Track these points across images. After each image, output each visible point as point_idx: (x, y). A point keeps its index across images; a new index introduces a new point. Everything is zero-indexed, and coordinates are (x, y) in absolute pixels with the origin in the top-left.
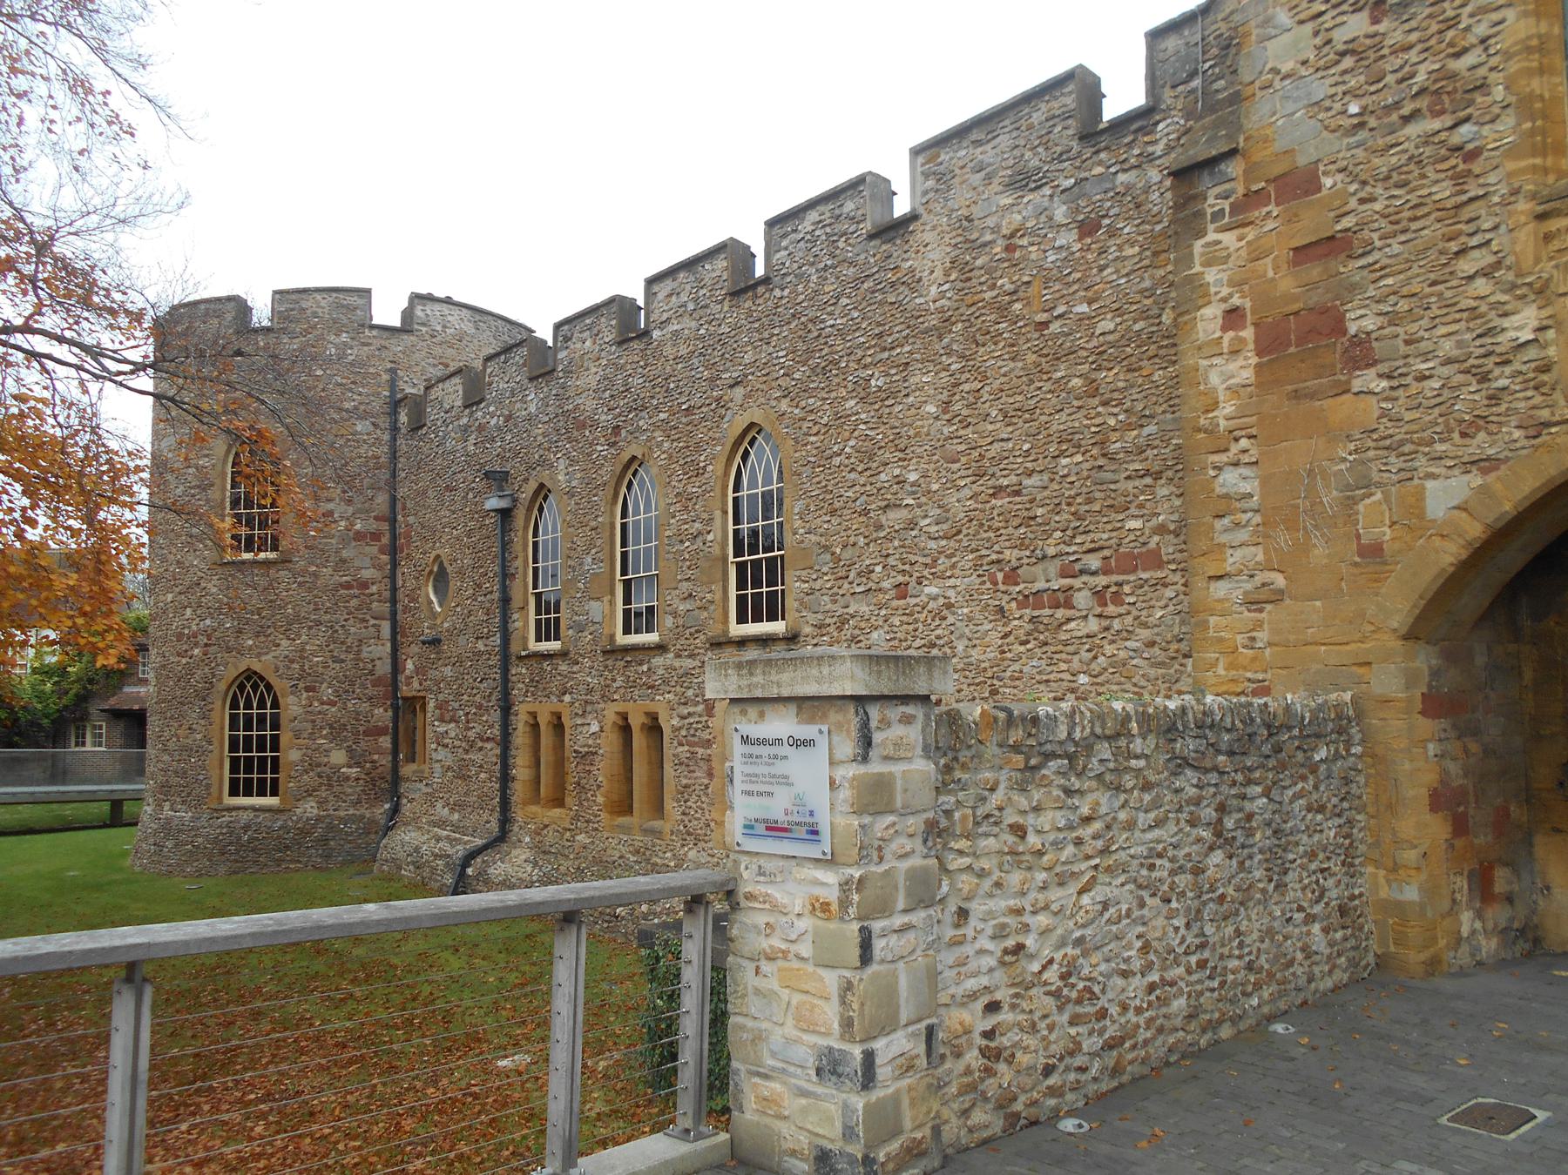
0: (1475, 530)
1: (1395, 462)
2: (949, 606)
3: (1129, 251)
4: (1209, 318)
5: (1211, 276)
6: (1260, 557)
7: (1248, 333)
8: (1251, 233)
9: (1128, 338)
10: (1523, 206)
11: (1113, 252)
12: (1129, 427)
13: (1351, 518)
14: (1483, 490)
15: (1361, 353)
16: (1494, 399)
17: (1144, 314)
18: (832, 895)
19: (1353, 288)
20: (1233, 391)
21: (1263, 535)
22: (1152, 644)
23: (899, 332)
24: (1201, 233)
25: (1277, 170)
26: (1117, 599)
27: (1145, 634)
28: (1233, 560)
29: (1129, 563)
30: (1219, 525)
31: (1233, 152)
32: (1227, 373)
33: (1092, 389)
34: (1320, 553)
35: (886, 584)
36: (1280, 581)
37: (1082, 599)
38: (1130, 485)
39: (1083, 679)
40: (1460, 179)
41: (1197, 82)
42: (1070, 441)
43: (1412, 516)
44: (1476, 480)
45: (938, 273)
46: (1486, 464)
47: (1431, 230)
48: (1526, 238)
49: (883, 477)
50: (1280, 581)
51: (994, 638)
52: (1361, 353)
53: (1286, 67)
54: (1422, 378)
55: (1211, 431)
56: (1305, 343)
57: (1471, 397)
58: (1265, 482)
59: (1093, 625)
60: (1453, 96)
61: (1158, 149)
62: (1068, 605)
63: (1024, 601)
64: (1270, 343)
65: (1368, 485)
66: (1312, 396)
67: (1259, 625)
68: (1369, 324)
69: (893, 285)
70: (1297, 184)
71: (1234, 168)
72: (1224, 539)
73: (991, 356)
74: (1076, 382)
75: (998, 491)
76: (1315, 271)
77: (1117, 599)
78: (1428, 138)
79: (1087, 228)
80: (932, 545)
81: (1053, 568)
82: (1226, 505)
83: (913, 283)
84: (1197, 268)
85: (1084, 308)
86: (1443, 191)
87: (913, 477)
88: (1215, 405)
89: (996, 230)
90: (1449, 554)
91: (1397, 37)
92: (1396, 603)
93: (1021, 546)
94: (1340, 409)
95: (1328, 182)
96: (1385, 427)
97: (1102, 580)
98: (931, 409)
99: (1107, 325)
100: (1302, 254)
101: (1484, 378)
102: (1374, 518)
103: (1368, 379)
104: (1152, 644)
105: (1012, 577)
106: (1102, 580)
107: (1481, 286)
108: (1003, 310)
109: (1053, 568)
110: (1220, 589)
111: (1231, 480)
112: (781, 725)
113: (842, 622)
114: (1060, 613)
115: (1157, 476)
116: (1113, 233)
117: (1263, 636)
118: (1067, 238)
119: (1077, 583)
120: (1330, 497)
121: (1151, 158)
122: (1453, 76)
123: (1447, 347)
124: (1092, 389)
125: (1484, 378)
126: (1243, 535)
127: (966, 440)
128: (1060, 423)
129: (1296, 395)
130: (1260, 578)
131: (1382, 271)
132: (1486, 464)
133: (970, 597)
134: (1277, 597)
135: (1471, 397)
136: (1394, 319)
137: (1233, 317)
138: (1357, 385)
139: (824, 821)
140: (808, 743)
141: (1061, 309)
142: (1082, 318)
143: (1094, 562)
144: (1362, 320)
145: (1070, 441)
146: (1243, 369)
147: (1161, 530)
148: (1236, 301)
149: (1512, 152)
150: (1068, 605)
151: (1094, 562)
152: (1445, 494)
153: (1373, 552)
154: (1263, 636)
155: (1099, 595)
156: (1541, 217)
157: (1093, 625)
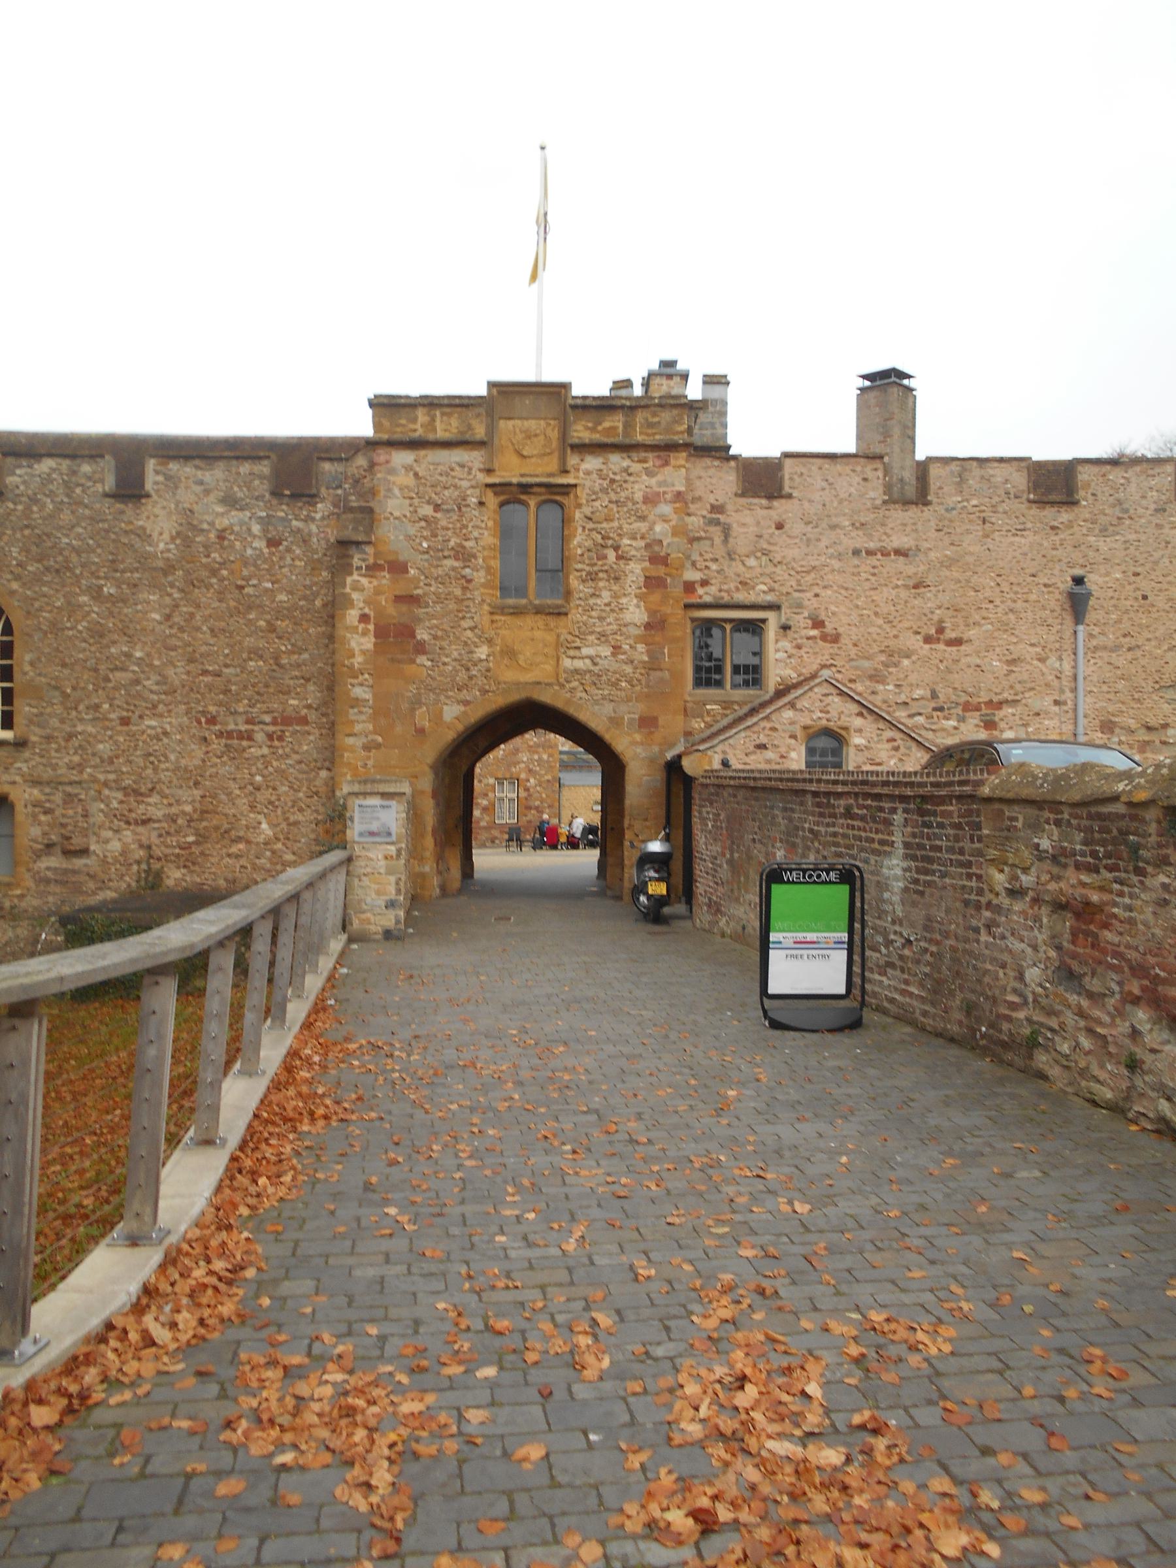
0: (460, 727)
1: (432, 696)
2: (165, 733)
3: (298, 563)
4: (352, 616)
5: (355, 596)
6: (371, 727)
7: (371, 627)
8: (375, 583)
9: (295, 607)
10: (486, 607)
11: (288, 561)
12: (294, 653)
13: (413, 716)
14: (465, 713)
15: (421, 648)
16: (471, 678)
17: (304, 598)
18: (394, 853)
19: (420, 620)
20: (363, 652)
21: (374, 717)
22: (300, 762)
23: (130, 561)
24: (351, 574)
25: (391, 558)
26: (281, 739)
27: (296, 757)
28: (358, 728)
29: (287, 721)
30: (351, 711)
31: (369, 543)
32: (360, 643)
33: (272, 628)
34: (399, 729)
35: (113, 716)
36: (380, 739)
37: (260, 737)
38: (291, 682)
39: (258, 778)
40: (464, 589)
41: (339, 492)
42: (256, 653)
43: (438, 717)
44: (462, 708)
45: (166, 536)
46: (466, 703)
47: (452, 606)
48: (486, 619)
49: (113, 650)
50: (380, 739)
51: (200, 754)
52: (421, 648)
53: (397, 514)
54: (445, 664)
55: (351, 667)
56: (396, 638)
57: (462, 676)
58: (375, 695)
59: (265, 751)
60: (463, 555)
61: (318, 516)
62: (250, 738)
63: (220, 735)
64: (381, 633)
65: (420, 703)
66: (399, 662)
67: (369, 758)
68: (426, 637)
69: (126, 532)
70: (398, 568)
71: (370, 550)
72: (352, 718)
73: (206, 597)
74: (262, 623)
75: (205, 672)
76: (404, 608)
77: (281, 739)
78: (454, 569)
79: (273, 543)
80: (155, 697)
81: (240, 719)
82: (356, 702)
83: (144, 536)
84: (348, 590)
85: (269, 585)
86: (458, 592)
87: (138, 654)
88: (353, 656)
89: (212, 524)
90: (450, 735)
91: (444, 523)
92: (430, 752)
93: (220, 704)
94: (410, 669)
95: (412, 572)
96: (429, 681)
97: (271, 728)
98: (157, 617)
99: (283, 597)
100: (398, 599)
101: (468, 669)
102: (422, 717)
103: (422, 660)
104: (300, 762)
105: (212, 721)
106: (271, 728)
107: (469, 633)
108: (214, 573)
109: (240, 719)
110: (350, 741)
111: (359, 692)
112: (375, 801)
113: (70, 737)
114: (245, 743)
115: (308, 680)
116: (288, 550)
117: (370, 763)
118: (260, 544)
119: (256, 728)
120: (405, 706)
121: (313, 519)
122: (464, 547)
123: (455, 654)
124: (272, 628)
125: (468, 669)
126: (363, 717)
127: (181, 639)
128: (249, 642)
129: (392, 660)
130: (370, 737)
131: (433, 617)
132: (466, 703)
133: (181, 729)
134: (378, 746)
135: (462, 676)
136: (435, 637)
137: (364, 618)
138: (418, 661)
139: (394, 830)
140: (388, 807)
141: (254, 582)
142: (267, 590)
143: (267, 718)
144: (422, 634)
145: (256, 653)
146: (368, 643)
147: (309, 707)
148: (367, 610)
149: (484, 586)
150: (250, 738)
151: (267, 718)
152: (451, 712)
153: (421, 731)
154: (370, 763)
155: (270, 737)
156: (492, 613)
157: (265, 751)
